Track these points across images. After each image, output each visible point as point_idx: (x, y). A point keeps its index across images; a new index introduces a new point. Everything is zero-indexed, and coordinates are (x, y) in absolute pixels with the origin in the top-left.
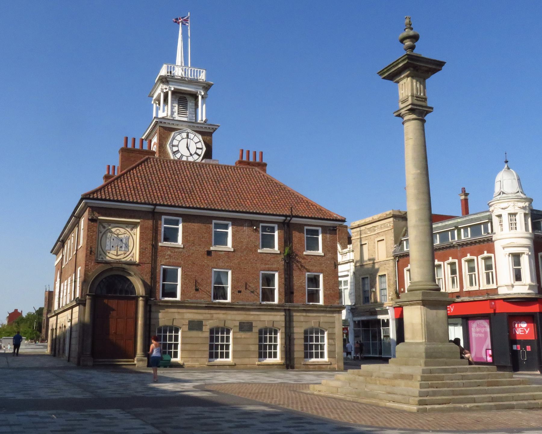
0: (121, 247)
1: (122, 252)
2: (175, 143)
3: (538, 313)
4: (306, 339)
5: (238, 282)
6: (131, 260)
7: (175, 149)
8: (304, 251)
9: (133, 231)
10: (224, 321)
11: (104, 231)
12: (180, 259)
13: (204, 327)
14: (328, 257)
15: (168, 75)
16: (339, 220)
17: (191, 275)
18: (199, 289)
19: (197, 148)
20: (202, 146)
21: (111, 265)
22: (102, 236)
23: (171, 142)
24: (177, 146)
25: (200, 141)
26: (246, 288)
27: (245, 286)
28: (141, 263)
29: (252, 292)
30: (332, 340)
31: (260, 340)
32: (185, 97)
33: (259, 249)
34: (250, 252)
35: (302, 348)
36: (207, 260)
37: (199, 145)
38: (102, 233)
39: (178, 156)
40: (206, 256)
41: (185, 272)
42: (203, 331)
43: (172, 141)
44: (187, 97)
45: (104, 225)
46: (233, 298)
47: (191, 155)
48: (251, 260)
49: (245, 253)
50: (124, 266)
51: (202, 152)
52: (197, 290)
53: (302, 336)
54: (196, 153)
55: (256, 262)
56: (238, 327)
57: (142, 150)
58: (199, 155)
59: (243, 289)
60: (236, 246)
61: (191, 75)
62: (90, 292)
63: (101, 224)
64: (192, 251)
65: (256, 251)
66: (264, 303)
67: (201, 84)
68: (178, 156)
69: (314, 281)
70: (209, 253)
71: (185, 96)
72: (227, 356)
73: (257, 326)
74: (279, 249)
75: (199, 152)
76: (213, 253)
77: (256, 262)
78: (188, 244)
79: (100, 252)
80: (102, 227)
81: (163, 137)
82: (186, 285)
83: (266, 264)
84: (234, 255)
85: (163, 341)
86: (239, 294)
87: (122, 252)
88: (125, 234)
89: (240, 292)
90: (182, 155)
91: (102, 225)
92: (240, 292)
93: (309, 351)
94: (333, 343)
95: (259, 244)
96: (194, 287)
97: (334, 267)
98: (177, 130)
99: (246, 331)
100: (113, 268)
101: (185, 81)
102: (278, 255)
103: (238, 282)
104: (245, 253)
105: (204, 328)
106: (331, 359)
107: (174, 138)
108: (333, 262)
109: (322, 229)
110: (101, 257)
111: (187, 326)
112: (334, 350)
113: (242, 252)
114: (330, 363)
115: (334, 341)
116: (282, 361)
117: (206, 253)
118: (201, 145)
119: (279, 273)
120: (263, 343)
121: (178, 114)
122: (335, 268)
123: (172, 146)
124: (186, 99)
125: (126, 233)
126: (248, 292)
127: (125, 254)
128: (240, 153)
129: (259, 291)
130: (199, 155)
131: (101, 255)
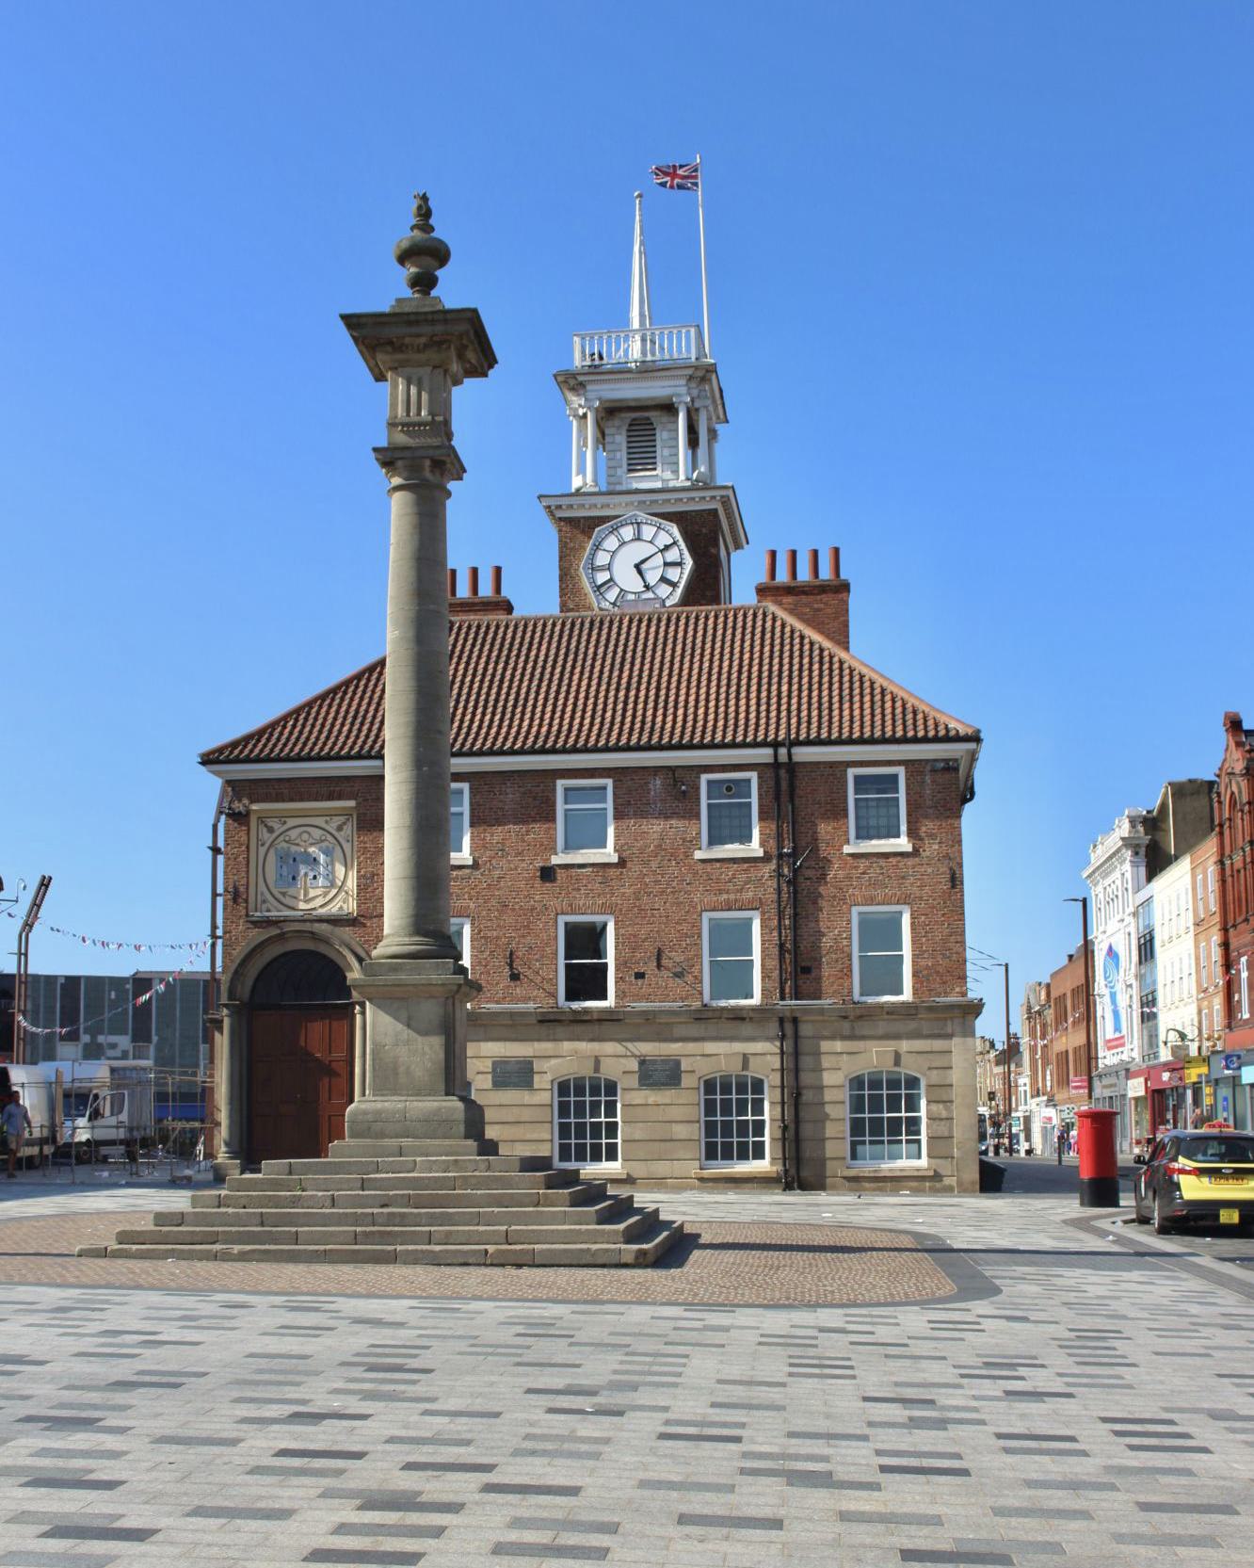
0: (315, 877)
1: (319, 892)
2: (602, 559)
3: (106, 1031)
4: (857, 1105)
5: (634, 950)
6: (341, 908)
7: (602, 577)
8: (848, 842)
9: (342, 833)
10: (593, 1059)
11: (271, 840)
12: (466, 897)
13: (536, 1078)
14: (928, 853)
15: (585, 363)
16: (958, 739)
17: (497, 938)
18: (522, 977)
19: (666, 564)
20: (681, 555)
21: (279, 928)
22: (266, 854)
23: (588, 558)
24: (609, 568)
25: (675, 543)
26: (659, 966)
27: (654, 959)
28: (362, 916)
29: (678, 975)
30: (941, 1106)
31: (710, 1108)
32: (648, 419)
33: (700, 849)
34: (669, 860)
35: (846, 1128)
36: (542, 892)
37: (672, 555)
38: (267, 845)
39: (612, 595)
40: (538, 882)
41: (480, 931)
42: (536, 1086)
43: (593, 555)
44: (652, 414)
45: (270, 824)
46: (620, 995)
47: (647, 587)
48: (674, 884)
49: (654, 865)
50: (318, 927)
51: (682, 575)
52: (515, 977)
53: (845, 1095)
54: (663, 579)
55: (689, 888)
56: (637, 1076)
57: (477, 600)
58: (674, 585)
59: (650, 968)
60: (626, 847)
61: (680, 351)
62: (230, 999)
63: (262, 822)
64: (497, 873)
65: (688, 855)
66: (576, 1005)
67: (679, 372)
68: (612, 595)
69: (884, 932)
70: (548, 874)
71: (646, 414)
72: (759, 1154)
73: (693, 1071)
74: (762, 844)
75: (673, 574)
76: (560, 874)
77: (689, 888)
78: (488, 853)
79: (262, 894)
80: (265, 830)
81: (571, 549)
82: (486, 966)
83: (721, 892)
84: (622, 873)
85: (721, 1116)
86: (640, 982)
87: (319, 892)
88: (322, 841)
89: (640, 976)
90: (622, 590)
91: (266, 826)
92: (640, 976)
93: (604, 1141)
94: (944, 1114)
95: (699, 833)
96: (507, 971)
97: (949, 885)
98: (604, 523)
99: (663, 1084)
100: (284, 933)
101: (630, 371)
102: (612, 872)
103: (634, 950)
104: (654, 865)
105: (687, 1081)
106: (933, 1161)
107: (597, 547)
108: (944, 869)
109: (907, 772)
110: (264, 906)
111: (490, 1076)
112: (946, 1134)
113: (646, 863)
114: (931, 1173)
115: (947, 1109)
116: (775, 1169)
117: (538, 874)
118: (682, 553)
119: (763, 914)
120: (588, 1120)
121: (630, 471)
122: (954, 886)
123: (593, 569)
124: (652, 424)
125: (326, 840)
126: (665, 973)
127: (325, 894)
128: (766, 560)
129: (701, 971)
130: (674, 585)
131: (264, 902)
